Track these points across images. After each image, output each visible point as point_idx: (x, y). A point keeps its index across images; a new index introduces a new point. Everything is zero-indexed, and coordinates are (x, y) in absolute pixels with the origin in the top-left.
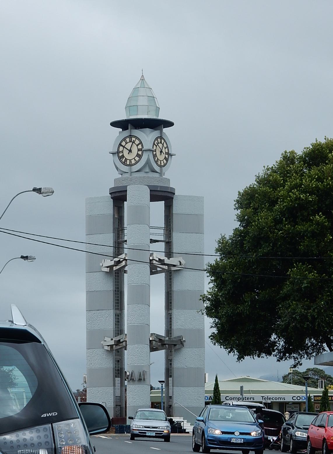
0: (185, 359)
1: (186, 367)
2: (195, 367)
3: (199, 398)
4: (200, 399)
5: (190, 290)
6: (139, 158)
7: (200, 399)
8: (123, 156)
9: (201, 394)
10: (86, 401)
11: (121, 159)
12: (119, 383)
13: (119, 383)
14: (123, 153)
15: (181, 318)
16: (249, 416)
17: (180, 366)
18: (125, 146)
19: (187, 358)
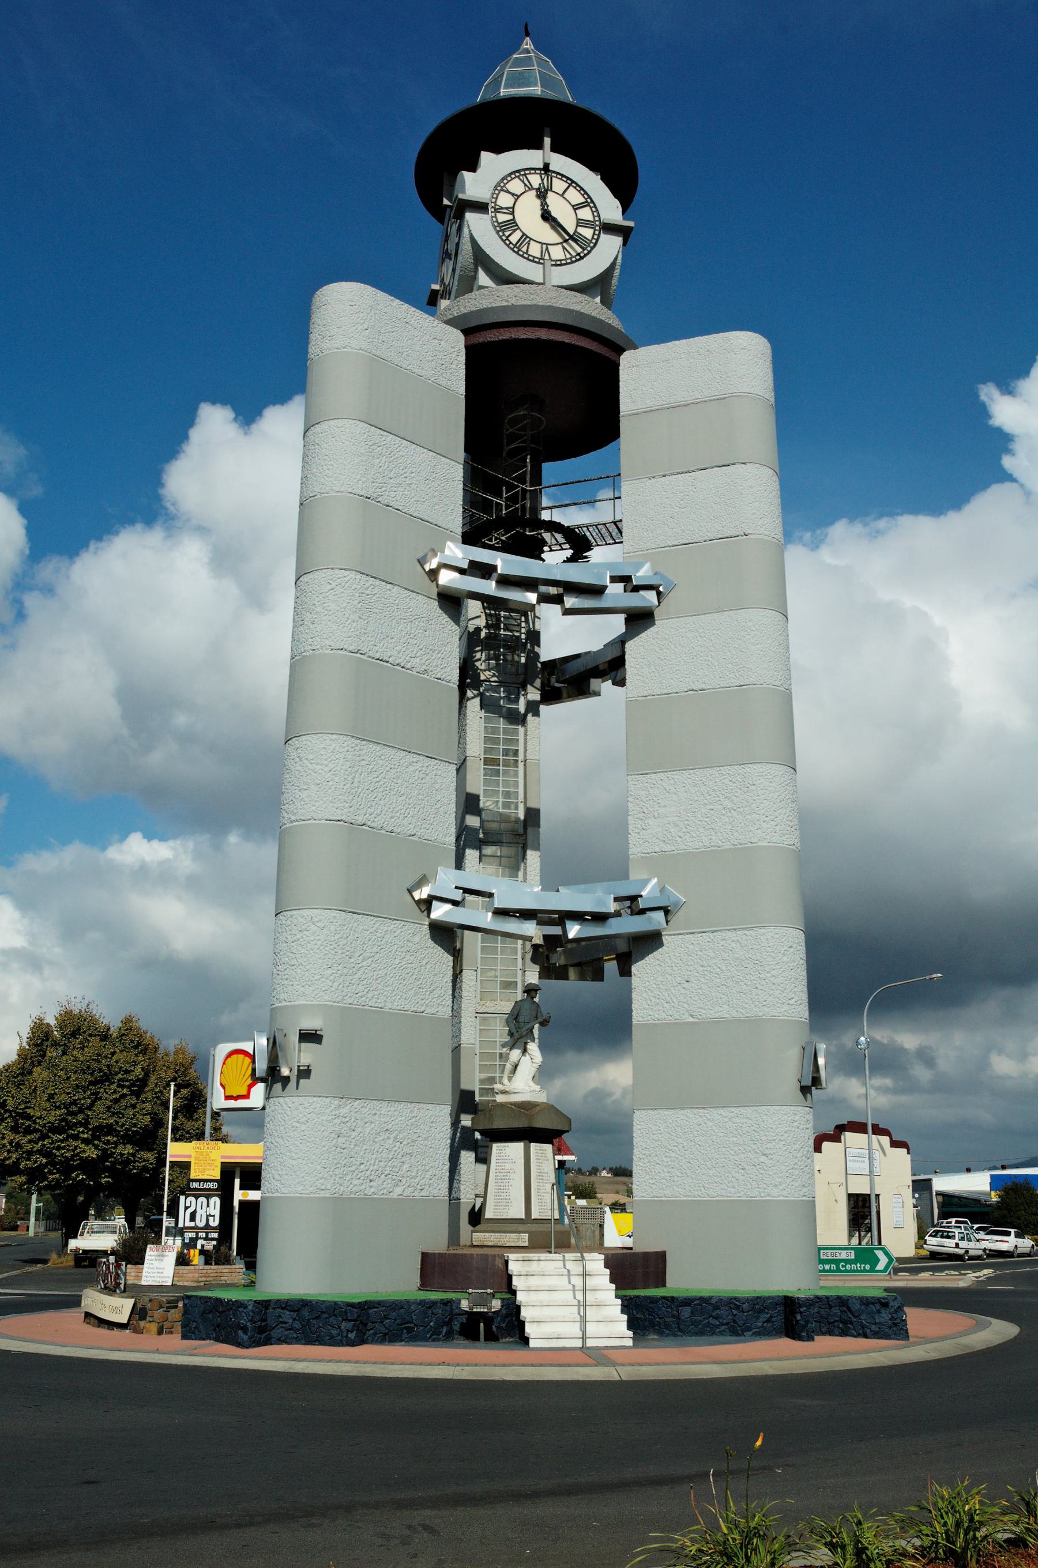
0: (686, 985)
1: (691, 1020)
2: (735, 1014)
3: (763, 1159)
4: (767, 1162)
5: (703, 686)
6: (515, 246)
7: (767, 1162)
8: (513, 225)
9: (770, 1142)
10: (175, 1140)
11: (503, 231)
12: (584, 1338)
13: (584, 1338)
14: (513, 213)
15: (662, 811)
16: (109, 681)
17: (664, 1016)
18: (508, 192)
19: (693, 979)
